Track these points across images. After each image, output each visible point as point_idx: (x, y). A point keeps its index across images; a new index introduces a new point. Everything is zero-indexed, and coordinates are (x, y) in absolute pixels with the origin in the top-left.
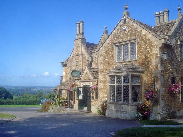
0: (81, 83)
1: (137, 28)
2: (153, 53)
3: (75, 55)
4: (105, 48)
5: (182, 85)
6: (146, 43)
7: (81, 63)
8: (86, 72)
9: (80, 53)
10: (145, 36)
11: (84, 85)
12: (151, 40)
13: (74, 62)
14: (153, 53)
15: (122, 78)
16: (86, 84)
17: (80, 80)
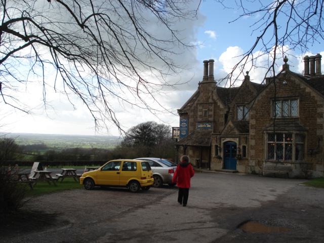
0: (222, 139)
1: (300, 85)
2: (318, 112)
3: (201, 101)
4: (258, 101)
5: (181, 1)
6: (310, 101)
7: (211, 113)
8: (230, 126)
9: (210, 101)
10: (309, 94)
11: (225, 141)
12: (316, 99)
13: (201, 111)
14: (318, 112)
15: (284, 136)
16: (228, 140)
17: (220, 135)
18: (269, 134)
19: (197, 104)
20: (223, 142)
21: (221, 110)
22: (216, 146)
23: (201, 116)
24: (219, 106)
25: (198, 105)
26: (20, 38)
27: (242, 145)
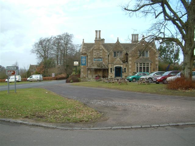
13: (95, 53)
18: (140, 63)
19: (93, 50)
20: (114, 67)
21: (106, 53)
22: (111, 69)
23: (95, 55)
24: (105, 51)
25: (94, 50)
26: (136, 9)
27: (124, 67)
